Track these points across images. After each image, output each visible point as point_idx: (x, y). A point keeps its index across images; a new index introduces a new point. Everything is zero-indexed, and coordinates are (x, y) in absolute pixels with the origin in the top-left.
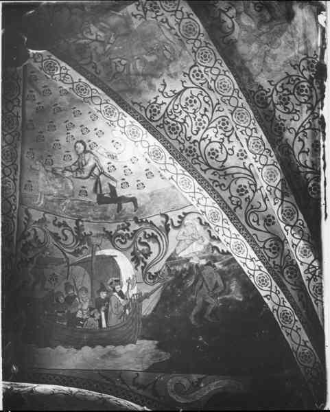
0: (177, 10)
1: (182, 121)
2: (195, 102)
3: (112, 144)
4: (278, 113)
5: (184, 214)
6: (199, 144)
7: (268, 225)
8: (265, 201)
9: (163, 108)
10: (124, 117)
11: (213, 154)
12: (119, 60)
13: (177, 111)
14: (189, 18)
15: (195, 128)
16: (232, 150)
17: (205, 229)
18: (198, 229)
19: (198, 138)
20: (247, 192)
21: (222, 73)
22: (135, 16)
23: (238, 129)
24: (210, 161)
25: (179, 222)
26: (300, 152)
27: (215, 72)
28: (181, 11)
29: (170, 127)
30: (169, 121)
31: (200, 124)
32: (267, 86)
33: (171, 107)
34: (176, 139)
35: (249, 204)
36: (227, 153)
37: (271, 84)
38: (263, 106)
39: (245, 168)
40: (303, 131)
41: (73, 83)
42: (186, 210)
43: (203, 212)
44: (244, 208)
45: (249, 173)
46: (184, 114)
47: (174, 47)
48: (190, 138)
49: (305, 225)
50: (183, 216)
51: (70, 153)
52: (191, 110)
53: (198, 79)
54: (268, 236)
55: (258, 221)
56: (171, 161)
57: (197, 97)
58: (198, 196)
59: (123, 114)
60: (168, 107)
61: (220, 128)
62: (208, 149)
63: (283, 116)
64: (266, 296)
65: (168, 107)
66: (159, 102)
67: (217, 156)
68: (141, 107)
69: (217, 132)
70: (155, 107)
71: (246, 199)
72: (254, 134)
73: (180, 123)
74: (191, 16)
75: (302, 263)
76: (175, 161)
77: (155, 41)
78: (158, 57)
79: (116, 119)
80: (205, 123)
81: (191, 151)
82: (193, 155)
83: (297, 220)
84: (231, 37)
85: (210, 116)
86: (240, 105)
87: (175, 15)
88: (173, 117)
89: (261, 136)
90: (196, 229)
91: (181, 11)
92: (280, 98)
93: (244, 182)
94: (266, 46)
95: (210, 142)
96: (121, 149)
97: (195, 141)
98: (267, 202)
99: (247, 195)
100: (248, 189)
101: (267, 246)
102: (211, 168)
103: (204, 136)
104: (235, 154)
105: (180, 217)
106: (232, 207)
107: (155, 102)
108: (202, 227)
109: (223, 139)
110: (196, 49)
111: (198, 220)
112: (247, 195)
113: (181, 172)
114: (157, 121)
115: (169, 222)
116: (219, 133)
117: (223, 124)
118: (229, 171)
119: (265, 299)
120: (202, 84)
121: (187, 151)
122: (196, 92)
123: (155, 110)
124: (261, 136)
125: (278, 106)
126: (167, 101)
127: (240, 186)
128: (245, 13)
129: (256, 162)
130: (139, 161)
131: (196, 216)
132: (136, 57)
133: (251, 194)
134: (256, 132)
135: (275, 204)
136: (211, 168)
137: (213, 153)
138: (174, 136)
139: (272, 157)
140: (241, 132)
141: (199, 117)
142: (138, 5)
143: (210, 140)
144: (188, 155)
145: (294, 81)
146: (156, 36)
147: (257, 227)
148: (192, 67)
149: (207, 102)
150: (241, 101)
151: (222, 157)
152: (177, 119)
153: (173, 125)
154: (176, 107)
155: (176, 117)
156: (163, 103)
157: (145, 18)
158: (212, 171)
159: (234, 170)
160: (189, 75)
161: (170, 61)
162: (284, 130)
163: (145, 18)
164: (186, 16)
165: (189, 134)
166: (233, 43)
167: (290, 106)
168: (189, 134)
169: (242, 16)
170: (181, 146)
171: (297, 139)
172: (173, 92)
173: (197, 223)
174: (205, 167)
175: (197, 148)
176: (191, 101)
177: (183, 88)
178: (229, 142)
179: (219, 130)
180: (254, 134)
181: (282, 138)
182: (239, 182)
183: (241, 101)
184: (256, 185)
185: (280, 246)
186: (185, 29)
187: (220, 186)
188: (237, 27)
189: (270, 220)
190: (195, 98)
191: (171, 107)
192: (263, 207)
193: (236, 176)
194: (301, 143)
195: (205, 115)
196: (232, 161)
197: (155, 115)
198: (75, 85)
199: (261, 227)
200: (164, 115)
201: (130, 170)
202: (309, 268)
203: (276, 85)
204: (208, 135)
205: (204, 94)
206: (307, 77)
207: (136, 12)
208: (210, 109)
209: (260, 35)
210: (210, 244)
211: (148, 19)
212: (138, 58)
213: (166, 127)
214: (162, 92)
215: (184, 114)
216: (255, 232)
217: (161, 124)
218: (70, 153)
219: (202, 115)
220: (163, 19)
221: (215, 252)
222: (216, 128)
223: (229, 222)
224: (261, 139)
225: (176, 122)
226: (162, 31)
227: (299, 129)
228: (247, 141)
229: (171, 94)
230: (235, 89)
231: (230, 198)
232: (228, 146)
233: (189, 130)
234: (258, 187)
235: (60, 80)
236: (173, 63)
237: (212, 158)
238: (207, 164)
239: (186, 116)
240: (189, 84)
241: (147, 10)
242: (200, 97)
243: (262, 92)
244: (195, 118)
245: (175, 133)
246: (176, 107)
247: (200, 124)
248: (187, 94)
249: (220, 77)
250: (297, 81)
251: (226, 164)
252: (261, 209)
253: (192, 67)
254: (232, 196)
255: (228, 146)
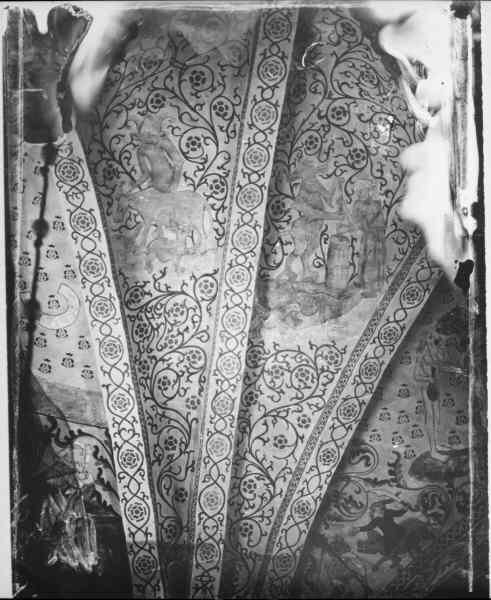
0: (249, 212)
1: (155, 326)
2: (182, 313)
3: (48, 299)
4: (261, 381)
5: (80, 431)
6: (156, 363)
7: (177, 500)
8: (187, 469)
9: (147, 298)
10: (106, 284)
11: (164, 384)
12: (136, 212)
13: (158, 312)
14: (254, 228)
15: (162, 342)
16: (185, 391)
17: (97, 464)
18: (87, 460)
19: (159, 355)
20: (174, 448)
21: (243, 306)
22: (186, 178)
23: (215, 375)
24: (157, 391)
25: (66, 438)
26: (258, 437)
27: (237, 300)
28: (252, 215)
29: (139, 325)
30: (144, 318)
31: (171, 342)
32: (268, 346)
33: (154, 303)
34: (138, 343)
35: (169, 464)
36: (178, 392)
37: (275, 347)
38: (252, 365)
39: (187, 421)
40: (274, 416)
41: (78, 207)
42: (85, 429)
43: (117, 446)
44: (162, 466)
45: (187, 426)
46: (162, 320)
47: (203, 241)
48: (152, 350)
49: (224, 523)
50: (76, 433)
51: (388, 411)
52: (171, 320)
53: (202, 292)
54: (171, 513)
55: (168, 490)
56: (124, 368)
57: (188, 310)
58: (125, 425)
59: (109, 281)
60: (150, 302)
61: (188, 358)
62: (161, 375)
63: (263, 388)
64: (138, 586)
65: (150, 302)
66: (146, 289)
67: (166, 389)
68: (126, 283)
69: (182, 361)
70: (138, 293)
71: (169, 456)
72: (230, 392)
73: (152, 327)
74: (257, 228)
75: (198, 565)
76: (129, 371)
77: (186, 219)
78: (177, 238)
79: (94, 280)
80: (176, 343)
81: (144, 367)
82: (144, 373)
83: (219, 513)
84: (270, 273)
85: (186, 340)
86: (236, 352)
87: (243, 215)
88: (149, 315)
89: (236, 398)
90: (85, 458)
91: (252, 215)
92: (274, 367)
93: (178, 435)
94: (297, 305)
95: (168, 368)
96: (55, 311)
97: (154, 357)
98: (189, 472)
99: (171, 452)
100: (177, 445)
101: (165, 525)
102: (153, 399)
103: (166, 358)
104: (186, 396)
105: (71, 432)
106: (153, 458)
107: (142, 287)
108: (94, 461)
109: (184, 373)
110: (234, 263)
111: (94, 449)
112: (171, 452)
113: (127, 388)
114: (131, 310)
115: (55, 432)
116: (183, 364)
117: (194, 356)
118: (169, 413)
119: (135, 589)
120: (203, 299)
121: (140, 363)
122: (191, 303)
123: (137, 296)
124: (236, 398)
125: (265, 374)
126: (156, 294)
127: (171, 438)
128: (302, 259)
129: (211, 422)
130: (67, 339)
131: (95, 442)
132: (154, 223)
133: (176, 453)
134: (233, 390)
135: (204, 481)
136: (153, 399)
137: (165, 383)
138: (138, 339)
139: (231, 426)
140: (217, 381)
141: (175, 333)
142: (200, 170)
143: (169, 365)
144: (140, 371)
145: (302, 360)
146: (192, 216)
147: (165, 496)
148: (207, 275)
149: (193, 322)
150: (240, 348)
151: (170, 392)
152: (152, 320)
153: (145, 325)
154: (159, 307)
155: (153, 317)
156: (149, 294)
157: (195, 189)
158: (153, 403)
159: (173, 415)
160: (196, 281)
161: (188, 253)
162: (254, 404)
163: (195, 189)
164: (252, 224)
165: (153, 346)
166: (267, 280)
167: (278, 382)
168: (153, 346)
169: (296, 260)
170: (138, 354)
171: (262, 421)
172: (168, 288)
173: (90, 451)
174: (148, 395)
175: (152, 366)
176: (178, 310)
177: (179, 290)
178: (188, 380)
179: (186, 361)
180: (230, 392)
181: (247, 411)
182: (173, 432)
183: (240, 348)
184: (187, 446)
185: (178, 530)
186: (241, 235)
187: (152, 425)
188: (282, 267)
189: (181, 495)
190: (185, 310)
191: (154, 303)
192: (182, 475)
193: (172, 423)
194: (265, 427)
195: (182, 334)
196: (178, 403)
197: (134, 302)
198: (79, 211)
199: (169, 500)
200: (142, 307)
201: (45, 341)
202: (203, 576)
203: (279, 352)
204: (170, 358)
205: (198, 311)
206: (319, 367)
207: (190, 174)
208: (192, 331)
209: (299, 291)
210: (93, 486)
211: (198, 191)
212: (156, 225)
213: (137, 322)
214: (156, 280)
215: (162, 320)
216: (162, 502)
217: (133, 316)
218: (388, 411)
219: (180, 333)
220: (215, 204)
221: (95, 499)
222: (184, 355)
223: (146, 477)
224: (233, 401)
225: (150, 323)
226: (203, 216)
227: (272, 411)
228: (217, 394)
229: (163, 288)
230: (242, 331)
231: (155, 446)
232: (184, 384)
233: (156, 340)
234: (188, 450)
235: (66, 194)
236: (190, 256)
237: (160, 388)
238: (152, 393)
239: (162, 323)
240: (189, 290)
241: (205, 182)
242: (191, 313)
243: (260, 349)
244: (169, 331)
245: (141, 336)
246: (159, 307)
247: (171, 342)
248: (179, 299)
249: (237, 309)
250: (305, 363)
251: (170, 404)
252: (178, 477)
253: (207, 275)
254: (158, 445)
255: (184, 384)
